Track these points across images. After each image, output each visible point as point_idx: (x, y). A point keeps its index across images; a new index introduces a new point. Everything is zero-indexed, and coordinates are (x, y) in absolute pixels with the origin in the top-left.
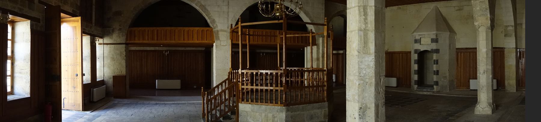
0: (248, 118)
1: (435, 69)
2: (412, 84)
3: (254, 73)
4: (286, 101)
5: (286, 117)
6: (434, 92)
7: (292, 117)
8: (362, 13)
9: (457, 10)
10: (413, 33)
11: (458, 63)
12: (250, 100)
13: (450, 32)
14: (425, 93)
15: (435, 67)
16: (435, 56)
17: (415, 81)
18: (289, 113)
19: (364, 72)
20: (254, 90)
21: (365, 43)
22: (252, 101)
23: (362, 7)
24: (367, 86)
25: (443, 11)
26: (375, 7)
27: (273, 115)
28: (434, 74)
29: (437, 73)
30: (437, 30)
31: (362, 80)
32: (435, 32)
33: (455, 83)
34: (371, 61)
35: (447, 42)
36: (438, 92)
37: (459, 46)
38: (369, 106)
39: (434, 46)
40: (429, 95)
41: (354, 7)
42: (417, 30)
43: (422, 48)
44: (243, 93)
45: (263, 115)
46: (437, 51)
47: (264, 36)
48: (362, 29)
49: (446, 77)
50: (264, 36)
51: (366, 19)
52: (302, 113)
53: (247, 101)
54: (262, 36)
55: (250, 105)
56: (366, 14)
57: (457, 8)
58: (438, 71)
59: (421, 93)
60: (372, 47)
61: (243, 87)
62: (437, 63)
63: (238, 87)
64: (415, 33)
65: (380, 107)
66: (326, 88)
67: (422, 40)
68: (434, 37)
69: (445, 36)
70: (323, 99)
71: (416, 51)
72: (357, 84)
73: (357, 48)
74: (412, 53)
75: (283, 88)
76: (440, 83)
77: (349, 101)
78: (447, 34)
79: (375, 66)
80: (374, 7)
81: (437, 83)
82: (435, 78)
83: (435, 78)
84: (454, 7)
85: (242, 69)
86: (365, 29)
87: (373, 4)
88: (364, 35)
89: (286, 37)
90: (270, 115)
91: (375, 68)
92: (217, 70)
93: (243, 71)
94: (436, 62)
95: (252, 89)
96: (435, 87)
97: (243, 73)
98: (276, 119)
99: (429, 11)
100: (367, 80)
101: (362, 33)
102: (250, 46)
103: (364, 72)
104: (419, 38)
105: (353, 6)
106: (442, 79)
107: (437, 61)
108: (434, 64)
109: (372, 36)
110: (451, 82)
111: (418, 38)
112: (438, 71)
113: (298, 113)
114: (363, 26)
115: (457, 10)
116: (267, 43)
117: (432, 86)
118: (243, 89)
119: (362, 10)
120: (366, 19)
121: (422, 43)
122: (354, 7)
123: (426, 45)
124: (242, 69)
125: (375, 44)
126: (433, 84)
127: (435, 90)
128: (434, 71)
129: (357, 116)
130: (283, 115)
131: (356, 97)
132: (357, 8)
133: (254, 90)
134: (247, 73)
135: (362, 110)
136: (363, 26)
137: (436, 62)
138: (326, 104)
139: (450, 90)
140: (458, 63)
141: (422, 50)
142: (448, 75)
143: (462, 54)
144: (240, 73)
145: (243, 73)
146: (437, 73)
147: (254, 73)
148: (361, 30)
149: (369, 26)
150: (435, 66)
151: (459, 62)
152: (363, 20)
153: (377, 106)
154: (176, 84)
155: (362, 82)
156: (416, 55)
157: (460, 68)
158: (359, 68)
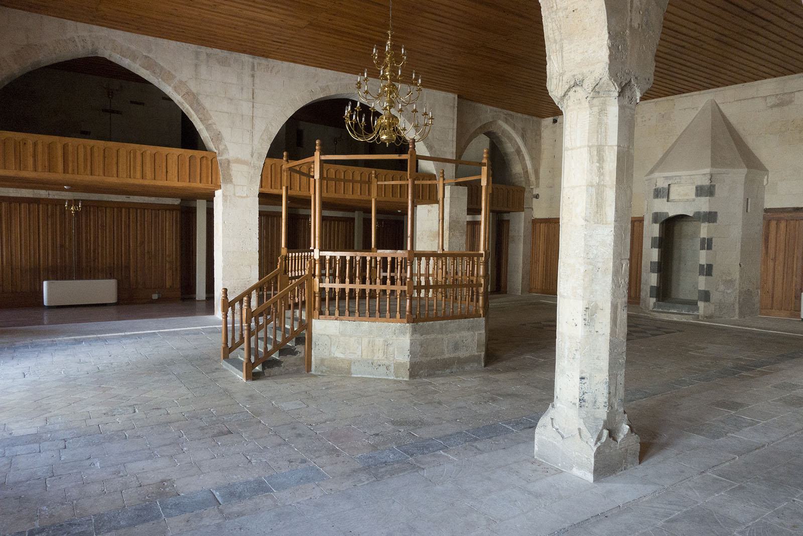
0: (333, 349)
1: (703, 261)
2: (643, 294)
3: (348, 258)
4: (411, 312)
5: (411, 344)
6: (697, 317)
7: (421, 345)
8: (596, 158)
9: (771, 107)
10: (652, 172)
11: (767, 248)
12: (337, 312)
13: (748, 167)
14: (675, 318)
15: (703, 257)
16: (704, 231)
17: (652, 287)
18: (417, 336)
19: (595, 252)
20: (347, 291)
21: (599, 205)
22: (342, 313)
23: (595, 148)
24: (599, 274)
25: (732, 111)
26: (619, 146)
27: (385, 341)
28: (701, 273)
29: (708, 270)
30: (713, 165)
31: (591, 264)
32: (708, 170)
33: (757, 299)
34: (608, 235)
35: (740, 194)
36: (709, 317)
37: (772, 201)
38: (600, 304)
39: (704, 205)
40: (684, 323)
41: (580, 147)
42: (661, 164)
43: (672, 211)
44: (323, 300)
45: (365, 341)
46: (711, 217)
47: (332, 179)
48: (595, 183)
49: (731, 282)
50: (332, 179)
51: (600, 168)
52: (440, 336)
53: (331, 314)
54: (353, 181)
55: (337, 323)
56: (601, 160)
57: (772, 101)
58: (710, 267)
59: (664, 317)
60: (610, 212)
61: (322, 285)
62: (709, 247)
63: (311, 286)
64: (656, 174)
65: (619, 309)
66: (482, 290)
67: (673, 189)
68: (706, 182)
69: (735, 178)
70: (477, 311)
71: (656, 217)
72: (582, 270)
73: (583, 215)
74: (646, 223)
75: (406, 288)
76: (715, 297)
77: (564, 297)
78: (739, 174)
79: (615, 242)
80: (616, 148)
81: (706, 296)
82: (702, 283)
83: (702, 283)
84: (765, 98)
85: (321, 250)
86: (598, 184)
87: (616, 143)
88: (597, 194)
89: (414, 186)
90: (379, 341)
91: (614, 246)
92: (225, 253)
93: (323, 253)
94: (707, 244)
95: (343, 290)
96: (701, 304)
97: (322, 259)
98: (391, 349)
99: (694, 114)
100: (600, 265)
101: (594, 190)
102: (289, 198)
103: (595, 252)
104: (666, 186)
105: (578, 145)
106: (722, 288)
107: (710, 241)
108: (702, 248)
109: (610, 195)
110: (746, 297)
111: (662, 184)
112: (710, 267)
113: (433, 336)
114: (596, 180)
115: (771, 107)
116: (336, 196)
117: (693, 304)
118: (322, 290)
119: (595, 153)
120: (600, 168)
121: (672, 197)
122: (580, 147)
123: (682, 200)
124: (321, 250)
125: (616, 208)
126: (695, 297)
127: (701, 311)
128: (702, 266)
129: (580, 320)
130: (405, 341)
131: (580, 291)
132: (586, 149)
133: (347, 291)
134: (352, 258)
135: (589, 311)
136: (596, 180)
137: (707, 244)
138: (482, 320)
139: (741, 314)
140: (767, 248)
141: (671, 215)
142: (737, 276)
143: (783, 225)
144: (317, 257)
145: (322, 259)
146: (708, 270)
147: (348, 258)
148: (592, 186)
149: (607, 178)
150: (703, 253)
151: (772, 244)
152: (595, 169)
153: (614, 308)
154: (104, 289)
155: (591, 267)
156: (657, 227)
157: (774, 260)
158: (585, 245)
